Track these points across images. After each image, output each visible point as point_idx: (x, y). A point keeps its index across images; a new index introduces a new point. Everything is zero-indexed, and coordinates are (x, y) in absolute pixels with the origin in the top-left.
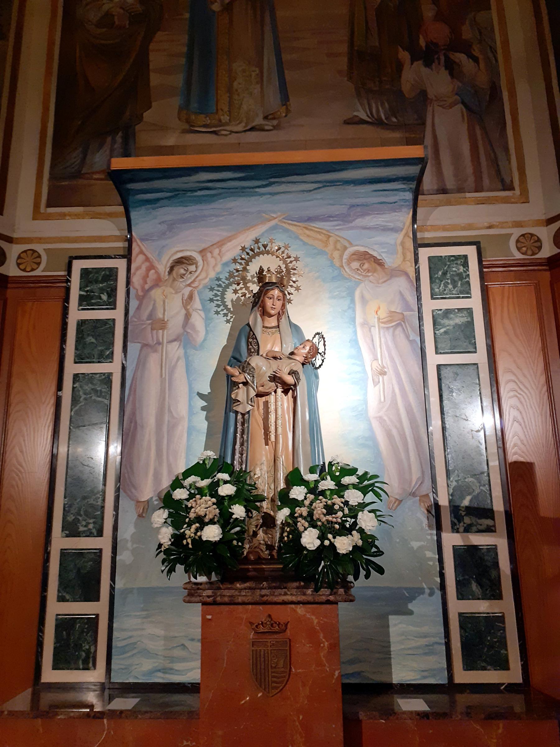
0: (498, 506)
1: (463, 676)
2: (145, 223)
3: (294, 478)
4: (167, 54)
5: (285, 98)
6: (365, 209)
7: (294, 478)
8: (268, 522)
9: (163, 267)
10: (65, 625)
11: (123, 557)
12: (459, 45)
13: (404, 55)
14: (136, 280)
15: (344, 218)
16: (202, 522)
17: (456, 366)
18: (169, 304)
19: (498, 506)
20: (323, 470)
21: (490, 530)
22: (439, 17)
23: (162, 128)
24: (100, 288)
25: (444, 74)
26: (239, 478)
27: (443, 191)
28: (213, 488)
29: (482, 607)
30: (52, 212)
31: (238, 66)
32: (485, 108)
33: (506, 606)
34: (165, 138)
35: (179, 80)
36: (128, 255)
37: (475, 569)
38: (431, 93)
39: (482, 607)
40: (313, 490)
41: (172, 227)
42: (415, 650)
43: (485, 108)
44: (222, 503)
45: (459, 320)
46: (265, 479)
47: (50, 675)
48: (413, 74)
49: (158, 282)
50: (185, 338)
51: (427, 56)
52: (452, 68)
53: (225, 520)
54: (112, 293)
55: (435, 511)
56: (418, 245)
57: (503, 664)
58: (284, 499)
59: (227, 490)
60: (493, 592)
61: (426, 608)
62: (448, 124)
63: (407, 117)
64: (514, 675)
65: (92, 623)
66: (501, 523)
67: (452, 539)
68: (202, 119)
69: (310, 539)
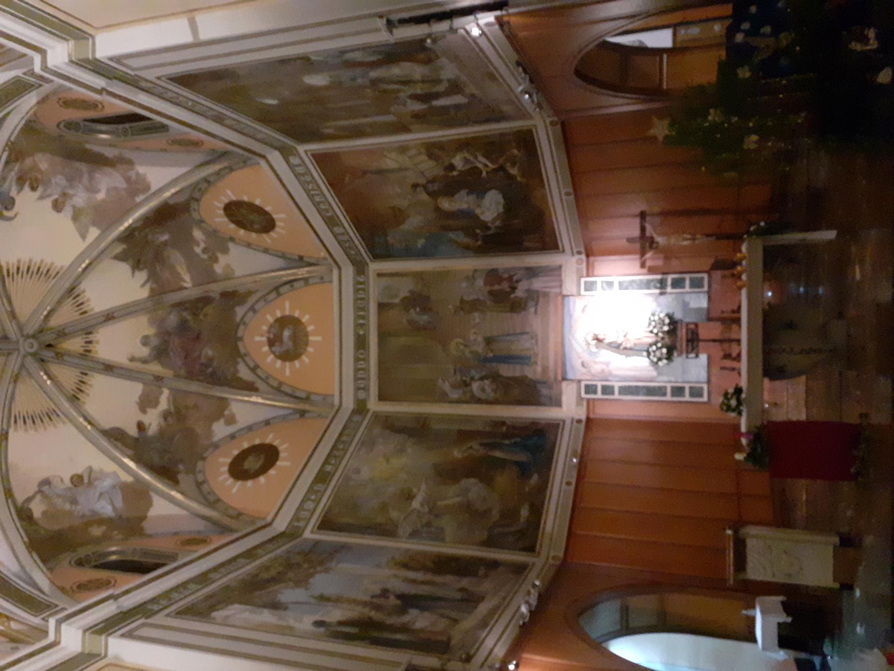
0: (659, 277)
1: (706, 288)
2: (570, 376)
3: (651, 332)
4: (506, 371)
5: (527, 333)
6: (569, 310)
7: (651, 332)
8: (663, 338)
9: (584, 370)
10: (691, 395)
11: (673, 379)
12: (510, 278)
13: (512, 296)
14: (588, 378)
15: (571, 316)
16: (662, 354)
17: (712, 344)
18: (597, 368)
19: (659, 277)
20: (650, 324)
21: (666, 280)
22: (499, 284)
23: (535, 371)
24: (590, 389)
25: (521, 283)
26: (651, 345)
27: (561, 286)
28: (654, 352)
29: (687, 282)
30: (312, 641)
31: (513, 347)
32: (532, 272)
33: (687, 277)
34: (533, 372)
35: (518, 367)
36: (579, 381)
37: (677, 284)
38: (527, 288)
39: (687, 282)
40: (654, 327)
41: (573, 368)
42: (700, 302)
43: (532, 272)
44: (658, 348)
45: (605, 285)
46: (651, 339)
47: (705, 398)
48: (520, 293)
49: (590, 372)
50: (607, 364)
51: (514, 289)
52: (518, 281)
53: (661, 348)
54: (592, 385)
55: (661, 294)
56: (579, 294)
57: (702, 278)
58: (657, 334)
59: (654, 348)
60: (683, 280)
61: (687, 298)
62: (538, 284)
63: (534, 297)
64: (705, 276)
65: (691, 388)
66: (665, 276)
67: (669, 289)
68: (533, 360)
69: (666, 328)
